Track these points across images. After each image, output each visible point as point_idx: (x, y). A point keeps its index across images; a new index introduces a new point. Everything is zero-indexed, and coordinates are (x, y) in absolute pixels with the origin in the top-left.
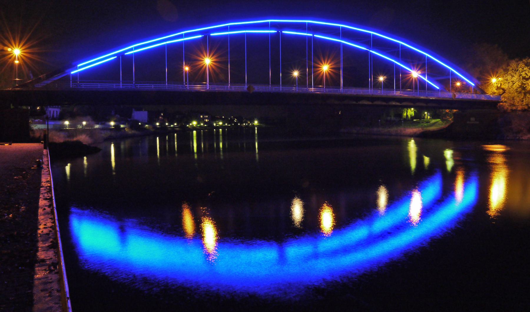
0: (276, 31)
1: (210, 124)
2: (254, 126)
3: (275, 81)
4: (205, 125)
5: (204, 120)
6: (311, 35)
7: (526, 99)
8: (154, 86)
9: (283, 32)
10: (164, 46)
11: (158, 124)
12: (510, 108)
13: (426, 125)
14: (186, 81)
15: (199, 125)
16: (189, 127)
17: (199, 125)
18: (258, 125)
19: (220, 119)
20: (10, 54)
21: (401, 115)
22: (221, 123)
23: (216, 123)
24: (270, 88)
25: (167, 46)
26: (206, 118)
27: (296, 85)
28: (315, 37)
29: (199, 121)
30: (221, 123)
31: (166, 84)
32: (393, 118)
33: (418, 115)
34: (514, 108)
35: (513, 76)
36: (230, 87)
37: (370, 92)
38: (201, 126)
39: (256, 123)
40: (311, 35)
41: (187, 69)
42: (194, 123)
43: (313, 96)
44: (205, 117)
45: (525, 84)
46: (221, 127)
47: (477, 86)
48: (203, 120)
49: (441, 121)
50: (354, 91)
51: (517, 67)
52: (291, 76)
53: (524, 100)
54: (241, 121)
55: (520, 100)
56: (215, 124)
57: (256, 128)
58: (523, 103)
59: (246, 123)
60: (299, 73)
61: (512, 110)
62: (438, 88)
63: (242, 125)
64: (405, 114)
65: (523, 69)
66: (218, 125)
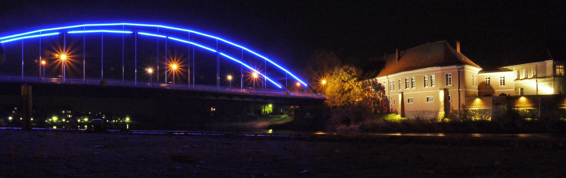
0: (132, 32)
1: (74, 119)
2: (125, 124)
3: (130, 76)
4: (68, 121)
5: (67, 116)
6: (165, 37)
7: (343, 98)
8: (10, 77)
9: (139, 33)
10: (21, 41)
11: (10, 118)
12: (332, 105)
13: (277, 119)
14: (42, 73)
15: (59, 121)
16: (48, 123)
17: (59, 121)
18: (130, 123)
19: (87, 115)
20: (58, 59)
21: (260, 111)
22: (86, 120)
23: (80, 119)
24: (123, 83)
25: (41, 39)
26: (69, 114)
27: (150, 80)
28: (169, 39)
29: (60, 116)
30: (86, 120)
31: (22, 76)
32: (253, 114)
33: (276, 112)
34: (334, 105)
35: (335, 79)
36: (84, 80)
37: (218, 89)
38: (62, 122)
39: (128, 119)
40: (165, 37)
41: (43, 62)
42: (55, 119)
43: (164, 90)
44: (68, 112)
45: (343, 86)
46: (86, 123)
47: (309, 86)
48: (65, 116)
49: (288, 117)
50: (200, 88)
51: (338, 72)
52: (226, 80)
53: (341, 98)
54: (110, 117)
55: (339, 98)
56: (79, 121)
57: (128, 125)
58: (340, 101)
59: (115, 120)
60: (255, 79)
61: (333, 106)
62: (280, 87)
63: (111, 122)
64: (263, 111)
65: (343, 73)
66: (83, 122)
